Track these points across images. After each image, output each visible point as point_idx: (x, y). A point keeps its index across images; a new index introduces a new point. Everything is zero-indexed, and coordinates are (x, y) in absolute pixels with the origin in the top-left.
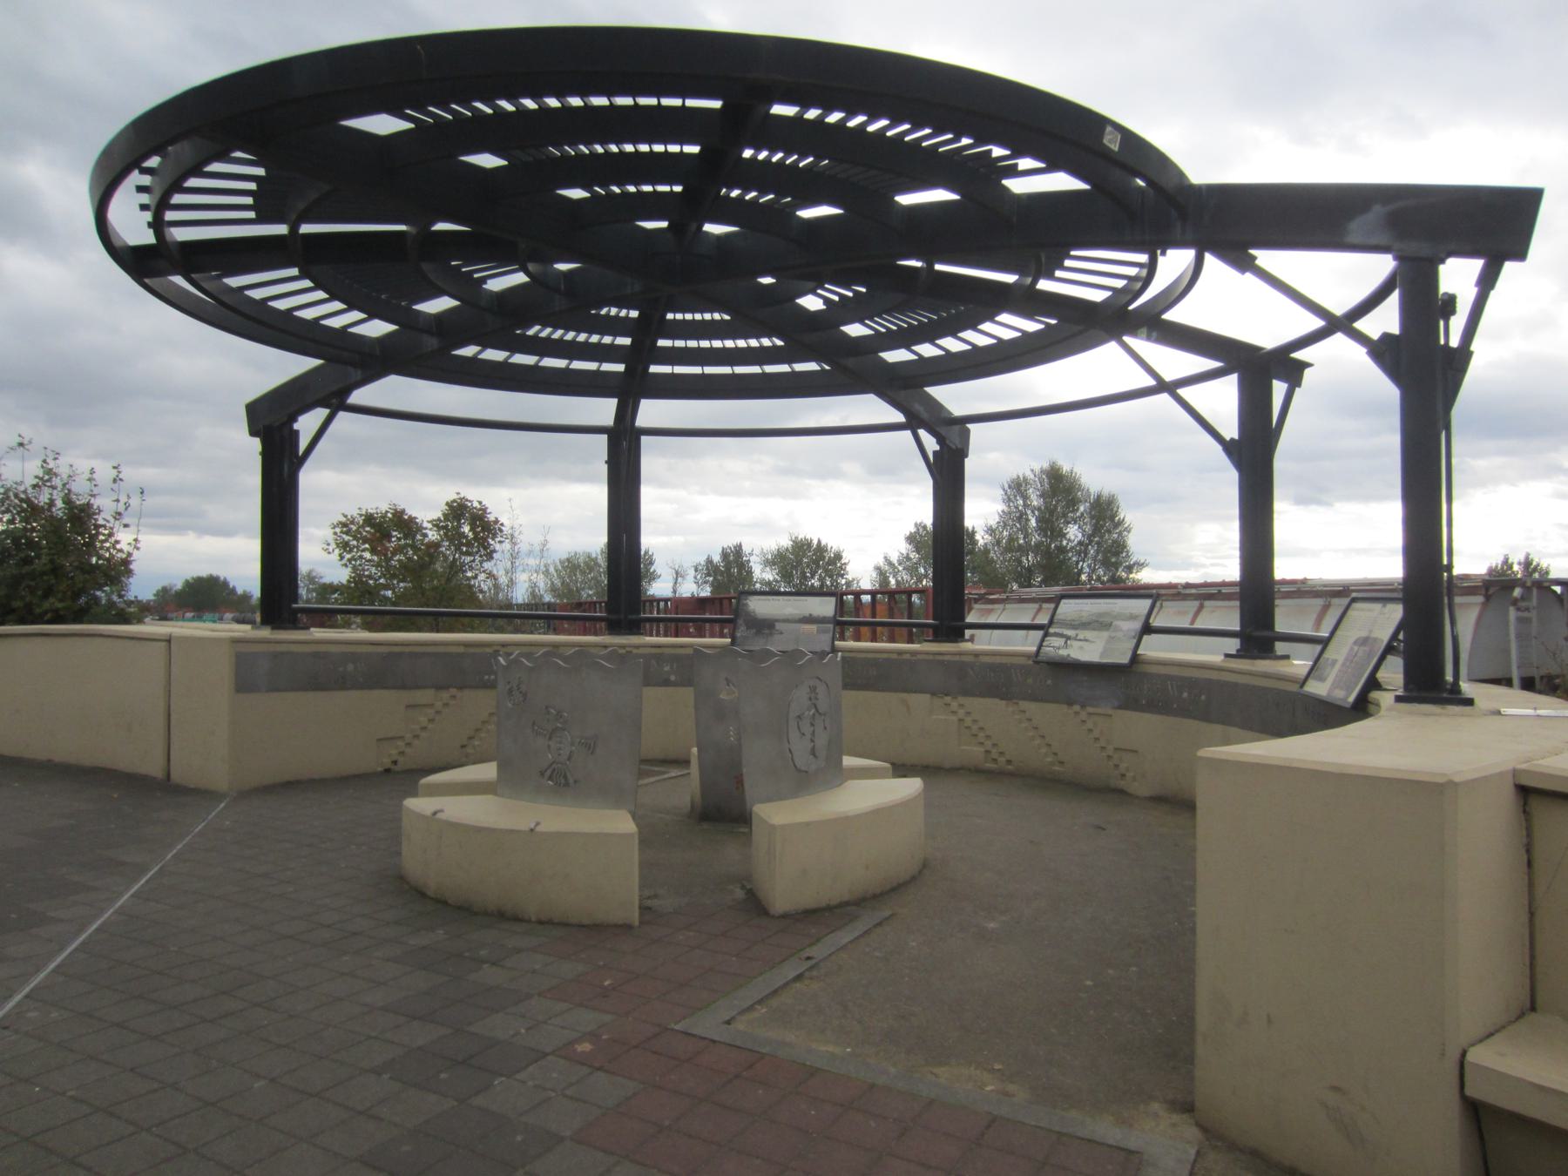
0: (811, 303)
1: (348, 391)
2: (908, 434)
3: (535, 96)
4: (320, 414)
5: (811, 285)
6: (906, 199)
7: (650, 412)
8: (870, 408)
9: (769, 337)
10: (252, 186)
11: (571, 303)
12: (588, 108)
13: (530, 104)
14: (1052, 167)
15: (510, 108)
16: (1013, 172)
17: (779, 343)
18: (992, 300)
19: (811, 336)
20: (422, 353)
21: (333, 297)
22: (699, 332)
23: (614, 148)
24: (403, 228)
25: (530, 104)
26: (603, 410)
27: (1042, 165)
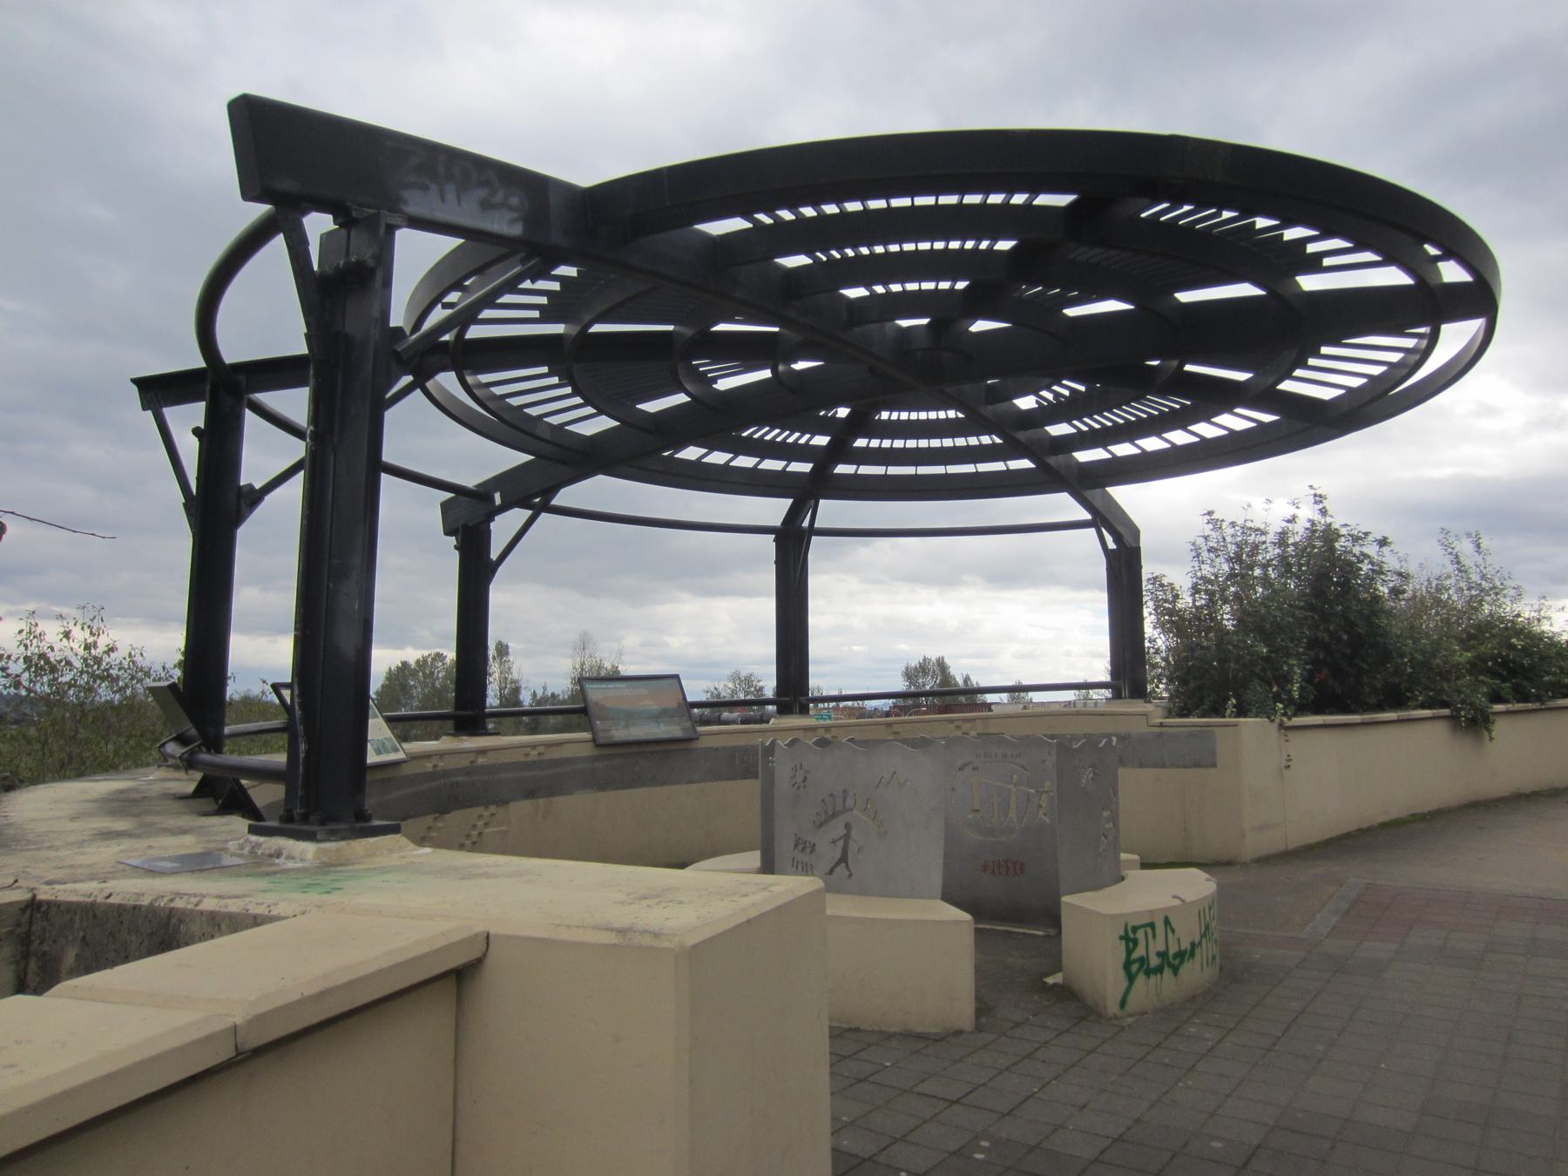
0: (1026, 403)
1: (554, 490)
2: (1093, 530)
3: (792, 207)
4: (519, 515)
5: (1047, 381)
6: (1184, 297)
7: (830, 511)
8: (1064, 505)
9: (989, 433)
10: (544, 300)
11: (788, 403)
12: (844, 214)
13: (786, 215)
14: (1387, 261)
15: (761, 217)
16: (1314, 264)
17: (998, 441)
18: (1223, 397)
19: (1020, 434)
20: (640, 453)
21: (587, 403)
22: (920, 425)
23: (865, 251)
24: (670, 328)
25: (786, 215)
26: (774, 510)
27: (1378, 258)
